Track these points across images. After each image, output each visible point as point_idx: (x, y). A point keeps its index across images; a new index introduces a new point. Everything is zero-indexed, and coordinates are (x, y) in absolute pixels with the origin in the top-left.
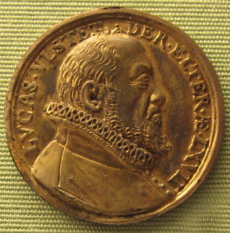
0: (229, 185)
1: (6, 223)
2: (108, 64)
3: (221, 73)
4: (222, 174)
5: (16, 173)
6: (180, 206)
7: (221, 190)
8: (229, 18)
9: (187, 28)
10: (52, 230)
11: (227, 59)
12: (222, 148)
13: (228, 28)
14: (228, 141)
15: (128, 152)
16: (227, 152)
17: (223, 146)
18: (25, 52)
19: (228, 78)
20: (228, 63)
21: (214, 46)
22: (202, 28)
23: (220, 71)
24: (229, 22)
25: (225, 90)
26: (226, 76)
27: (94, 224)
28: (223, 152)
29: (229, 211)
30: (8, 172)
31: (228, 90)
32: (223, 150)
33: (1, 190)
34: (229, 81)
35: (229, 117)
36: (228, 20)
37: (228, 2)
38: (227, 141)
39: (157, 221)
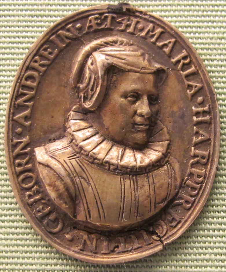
1: (30, 258)
7: (212, 208)
10: (69, 267)
15: (36, 56)
20: (223, 218)
24: (225, 54)
25: (218, 88)
27: (85, 264)
29: (224, 24)
30: (11, 224)
31: (222, 88)
32: (217, 188)
36: (224, 52)
37: (222, 2)
39: (151, 261)
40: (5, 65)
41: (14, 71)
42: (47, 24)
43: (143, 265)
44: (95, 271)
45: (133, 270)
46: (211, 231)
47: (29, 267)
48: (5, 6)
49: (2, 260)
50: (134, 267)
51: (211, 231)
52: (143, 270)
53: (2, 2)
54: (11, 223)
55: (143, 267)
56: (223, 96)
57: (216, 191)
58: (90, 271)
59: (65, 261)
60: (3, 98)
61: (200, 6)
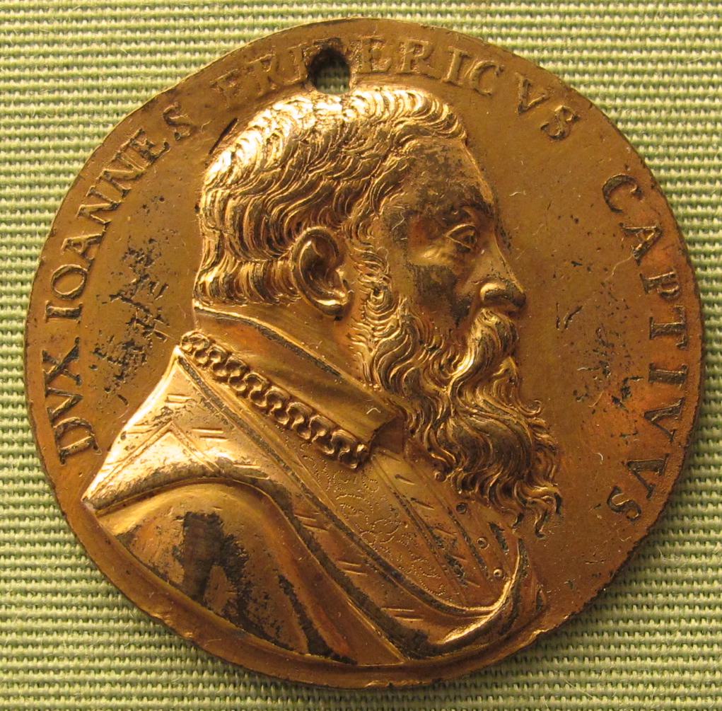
0: (720, 506)
2: (458, 227)
3: (627, 64)
4: (692, 505)
5: (36, 473)
6: (486, 672)
8: (719, 37)
9: (519, 42)
11: (711, 581)
12: (682, 486)
13: (718, 42)
14: (716, 400)
16: (716, 432)
17: (691, 456)
18: (67, 188)
19: (717, 247)
21: (617, 19)
22: (578, 19)
23: (683, 205)
26: (712, 242)
28: (696, 458)
32: (691, 479)
33: (2, 82)
34: (718, 529)
35: (718, 363)
38: (716, 400)
40: (39, 506)
41: (32, 258)
42: (159, 81)
43: (300, 694)
44: (399, 709)
45: (405, 705)
46: (652, 623)
47: (155, 702)
48: (15, 176)
49: (4, 251)
50: (419, 699)
51: (652, 623)
52: (415, 704)
53: (7, 3)
54: (18, 214)
55: (448, 700)
56: (717, 309)
57: (672, 535)
58: (409, 709)
59: (231, 688)
60: (5, 293)
61: (659, 87)
